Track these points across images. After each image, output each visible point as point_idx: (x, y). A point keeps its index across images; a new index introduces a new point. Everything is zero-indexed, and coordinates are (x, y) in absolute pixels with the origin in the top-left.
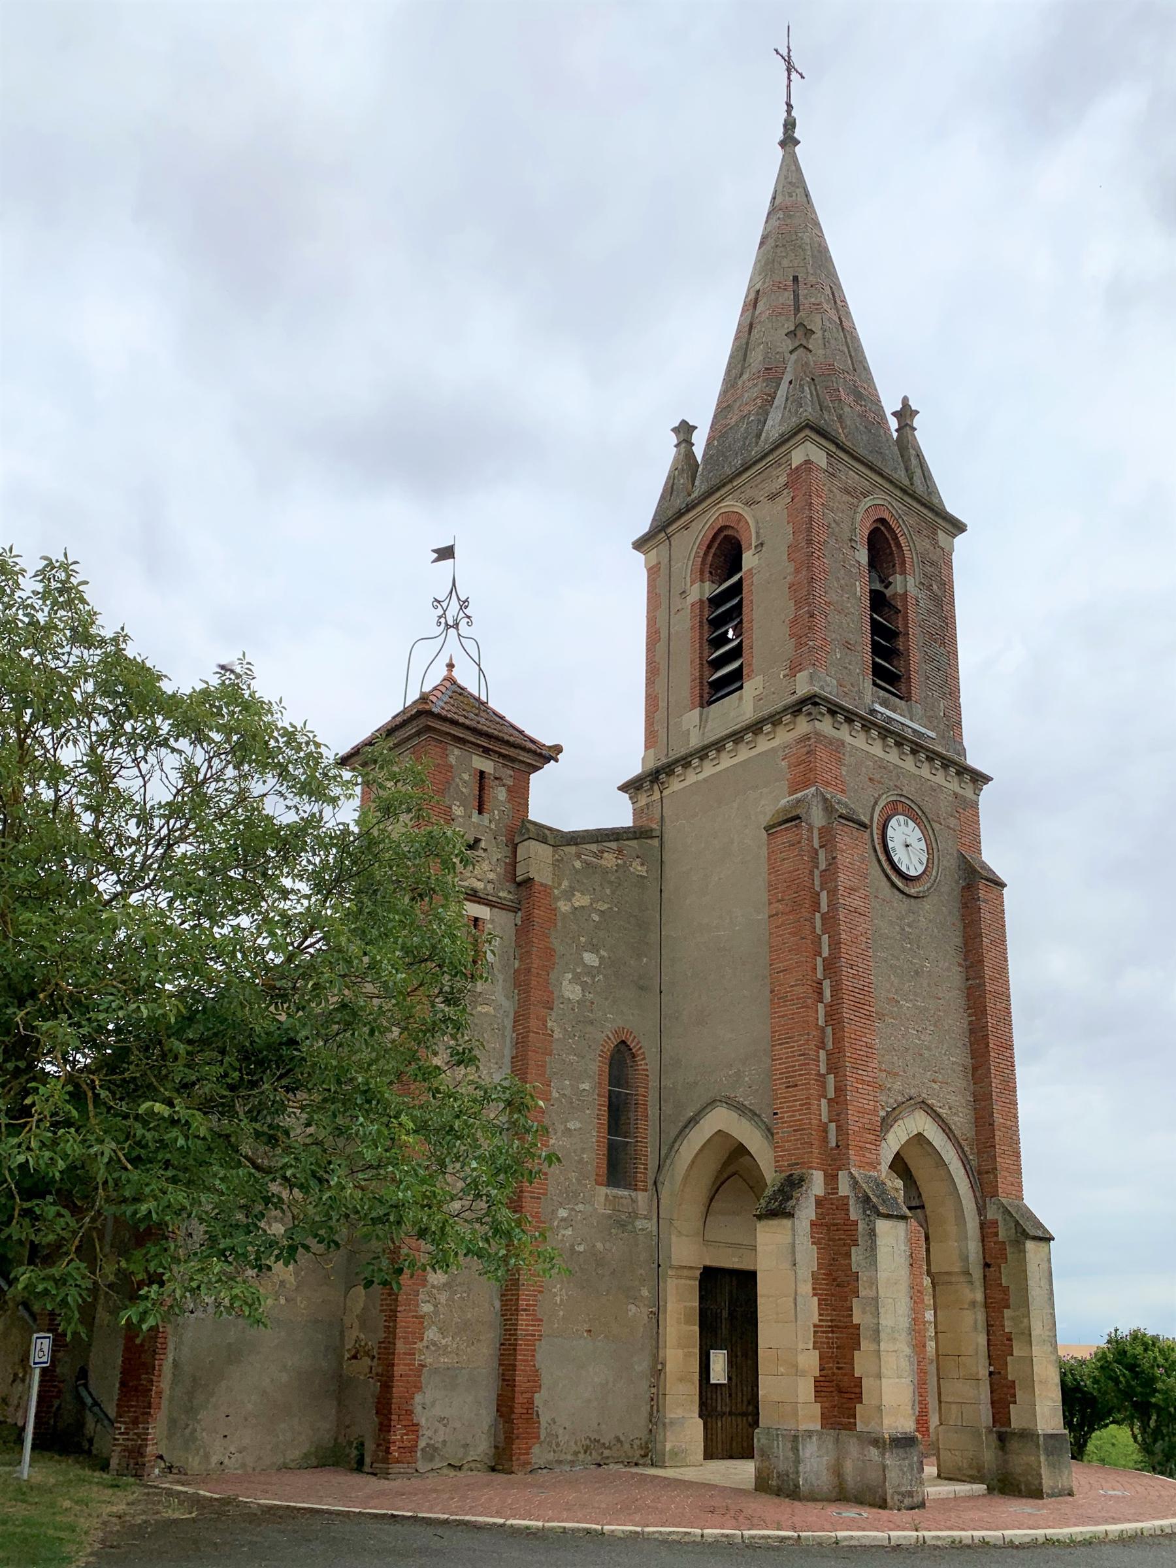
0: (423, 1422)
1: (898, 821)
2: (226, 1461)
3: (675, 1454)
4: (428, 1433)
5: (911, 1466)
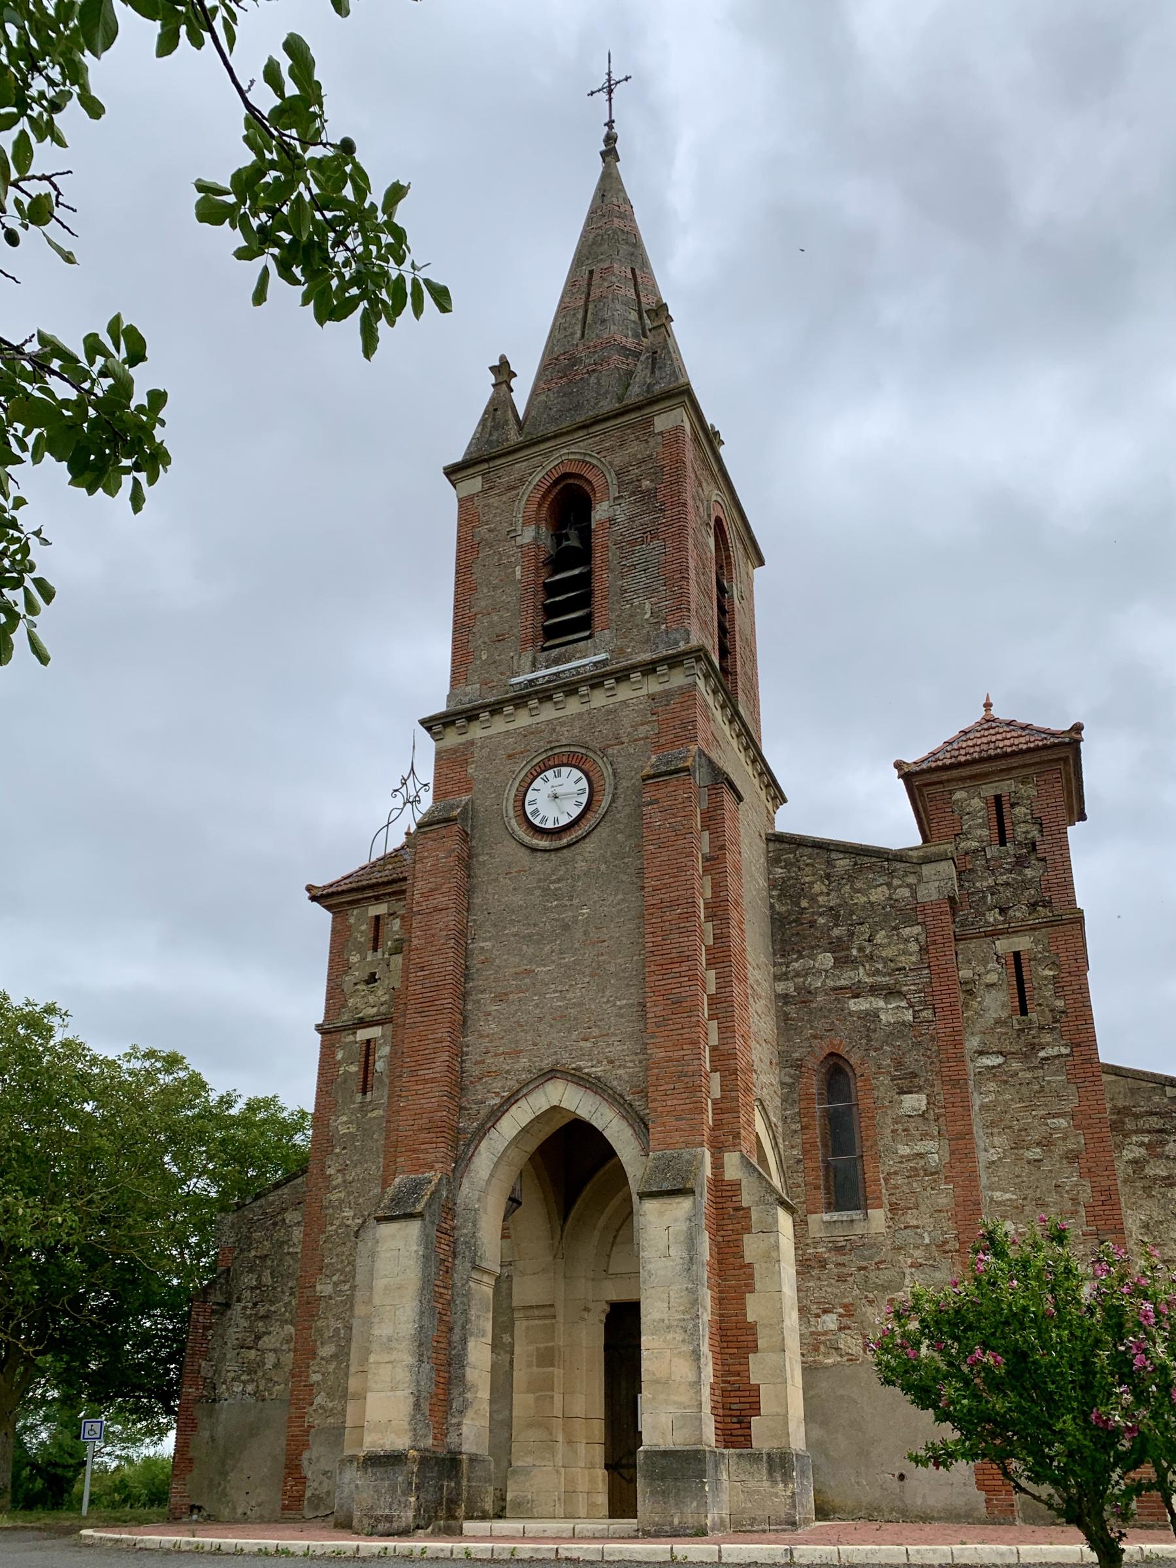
0: (309, 1475)
1: (580, 779)
2: (249, 1513)
3: (518, 1505)
4: (315, 1485)
5: (393, 1488)
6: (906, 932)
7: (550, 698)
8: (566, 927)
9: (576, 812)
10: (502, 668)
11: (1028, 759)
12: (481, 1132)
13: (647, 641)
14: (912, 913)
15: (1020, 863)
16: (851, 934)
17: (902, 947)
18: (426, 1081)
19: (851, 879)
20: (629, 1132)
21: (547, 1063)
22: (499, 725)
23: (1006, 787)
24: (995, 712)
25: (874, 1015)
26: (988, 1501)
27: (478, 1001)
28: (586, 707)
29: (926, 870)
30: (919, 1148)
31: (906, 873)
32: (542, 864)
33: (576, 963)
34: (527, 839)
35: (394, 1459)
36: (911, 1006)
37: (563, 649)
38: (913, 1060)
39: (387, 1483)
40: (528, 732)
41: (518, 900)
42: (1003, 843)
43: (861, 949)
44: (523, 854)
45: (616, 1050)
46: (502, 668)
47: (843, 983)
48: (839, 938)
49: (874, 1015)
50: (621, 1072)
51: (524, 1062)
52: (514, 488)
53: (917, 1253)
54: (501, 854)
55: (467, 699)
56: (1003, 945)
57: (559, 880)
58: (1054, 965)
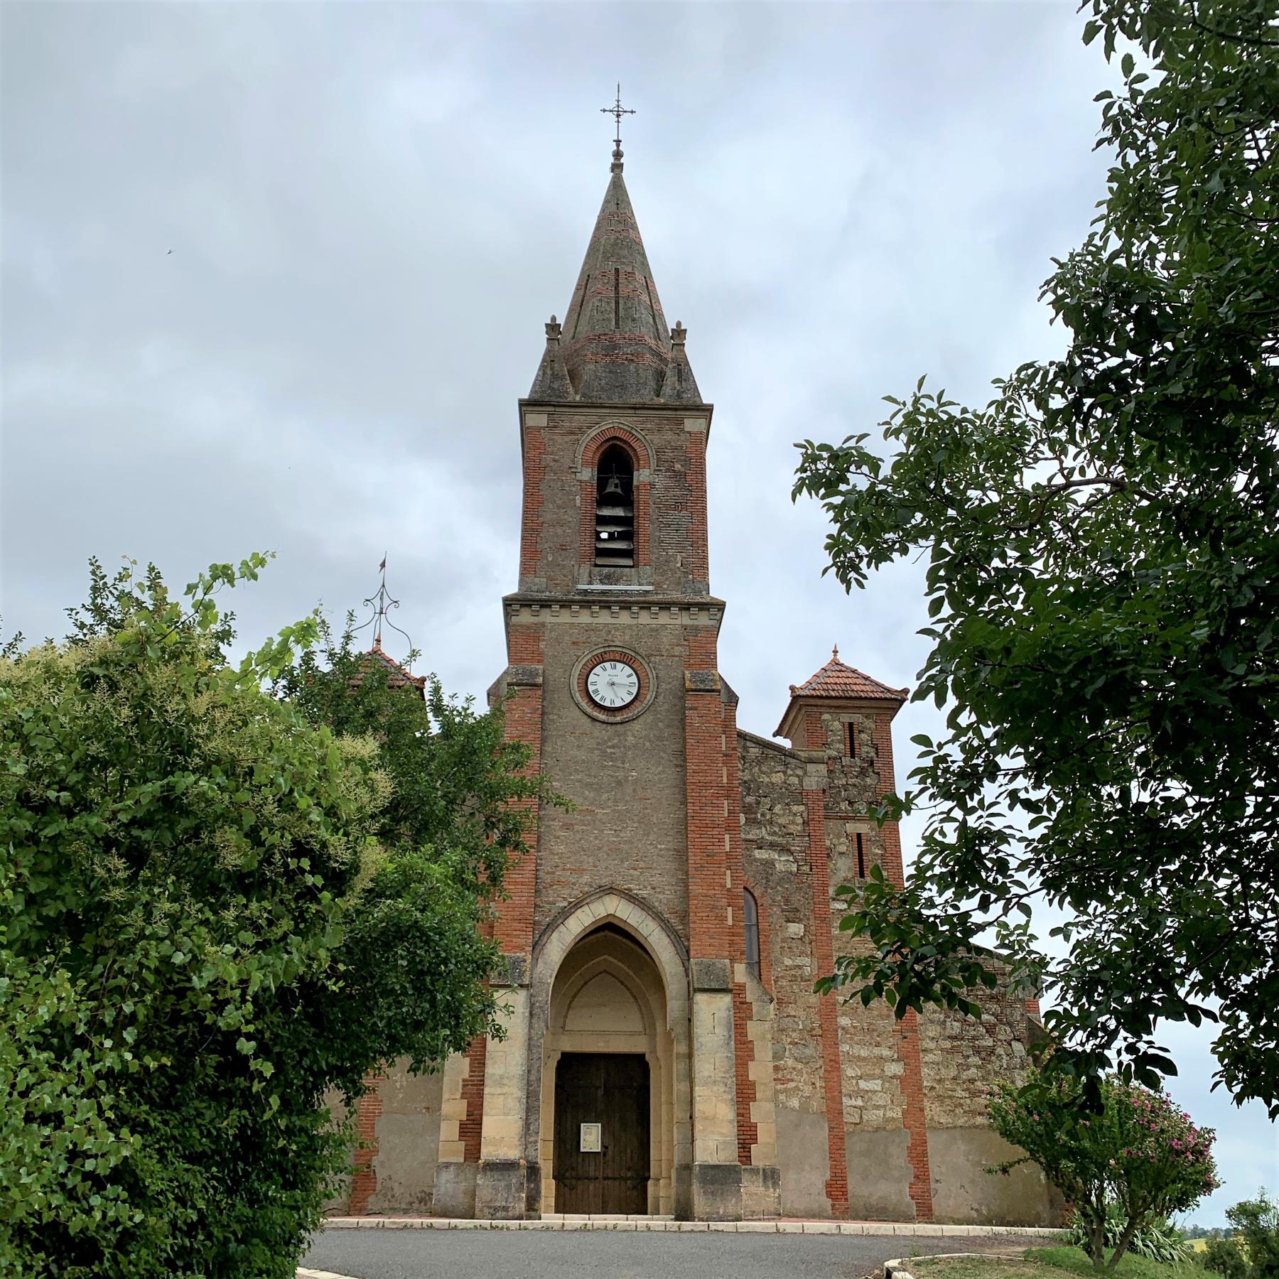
5: (508, 1187)
6: (795, 808)
7: (609, 608)
8: (619, 783)
9: (628, 699)
10: (565, 572)
11: (873, 703)
12: (551, 927)
13: (679, 584)
14: (799, 796)
15: (863, 773)
16: (758, 803)
17: (791, 817)
18: (516, 883)
19: (759, 763)
20: (667, 940)
21: (605, 881)
22: (565, 617)
23: (857, 718)
24: (842, 658)
25: (771, 863)
26: (833, 1206)
27: (549, 826)
28: (634, 622)
29: (810, 767)
30: (799, 961)
31: (796, 767)
32: (600, 732)
33: (628, 811)
34: (589, 710)
35: (509, 1166)
36: (796, 861)
37: (612, 570)
38: (796, 899)
39: (503, 1183)
40: (588, 629)
41: (581, 755)
42: (853, 756)
43: (763, 815)
44: (584, 719)
45: (656, 880)
46: (565, 572)
47: (750, 837)
48: (750, 804)
49: (771, 863)
50: (661, 896)
51: (586, 878)
52: (574, 434)
53: (794, 1035)
54: (569, 717)
55: (535, 588)
56: (852, 827)
57: (613, 747)
58: (883, 847)
